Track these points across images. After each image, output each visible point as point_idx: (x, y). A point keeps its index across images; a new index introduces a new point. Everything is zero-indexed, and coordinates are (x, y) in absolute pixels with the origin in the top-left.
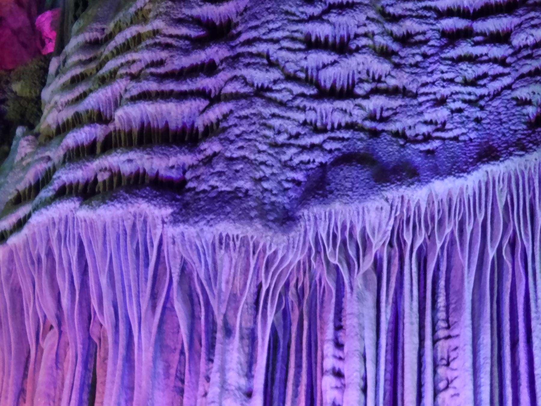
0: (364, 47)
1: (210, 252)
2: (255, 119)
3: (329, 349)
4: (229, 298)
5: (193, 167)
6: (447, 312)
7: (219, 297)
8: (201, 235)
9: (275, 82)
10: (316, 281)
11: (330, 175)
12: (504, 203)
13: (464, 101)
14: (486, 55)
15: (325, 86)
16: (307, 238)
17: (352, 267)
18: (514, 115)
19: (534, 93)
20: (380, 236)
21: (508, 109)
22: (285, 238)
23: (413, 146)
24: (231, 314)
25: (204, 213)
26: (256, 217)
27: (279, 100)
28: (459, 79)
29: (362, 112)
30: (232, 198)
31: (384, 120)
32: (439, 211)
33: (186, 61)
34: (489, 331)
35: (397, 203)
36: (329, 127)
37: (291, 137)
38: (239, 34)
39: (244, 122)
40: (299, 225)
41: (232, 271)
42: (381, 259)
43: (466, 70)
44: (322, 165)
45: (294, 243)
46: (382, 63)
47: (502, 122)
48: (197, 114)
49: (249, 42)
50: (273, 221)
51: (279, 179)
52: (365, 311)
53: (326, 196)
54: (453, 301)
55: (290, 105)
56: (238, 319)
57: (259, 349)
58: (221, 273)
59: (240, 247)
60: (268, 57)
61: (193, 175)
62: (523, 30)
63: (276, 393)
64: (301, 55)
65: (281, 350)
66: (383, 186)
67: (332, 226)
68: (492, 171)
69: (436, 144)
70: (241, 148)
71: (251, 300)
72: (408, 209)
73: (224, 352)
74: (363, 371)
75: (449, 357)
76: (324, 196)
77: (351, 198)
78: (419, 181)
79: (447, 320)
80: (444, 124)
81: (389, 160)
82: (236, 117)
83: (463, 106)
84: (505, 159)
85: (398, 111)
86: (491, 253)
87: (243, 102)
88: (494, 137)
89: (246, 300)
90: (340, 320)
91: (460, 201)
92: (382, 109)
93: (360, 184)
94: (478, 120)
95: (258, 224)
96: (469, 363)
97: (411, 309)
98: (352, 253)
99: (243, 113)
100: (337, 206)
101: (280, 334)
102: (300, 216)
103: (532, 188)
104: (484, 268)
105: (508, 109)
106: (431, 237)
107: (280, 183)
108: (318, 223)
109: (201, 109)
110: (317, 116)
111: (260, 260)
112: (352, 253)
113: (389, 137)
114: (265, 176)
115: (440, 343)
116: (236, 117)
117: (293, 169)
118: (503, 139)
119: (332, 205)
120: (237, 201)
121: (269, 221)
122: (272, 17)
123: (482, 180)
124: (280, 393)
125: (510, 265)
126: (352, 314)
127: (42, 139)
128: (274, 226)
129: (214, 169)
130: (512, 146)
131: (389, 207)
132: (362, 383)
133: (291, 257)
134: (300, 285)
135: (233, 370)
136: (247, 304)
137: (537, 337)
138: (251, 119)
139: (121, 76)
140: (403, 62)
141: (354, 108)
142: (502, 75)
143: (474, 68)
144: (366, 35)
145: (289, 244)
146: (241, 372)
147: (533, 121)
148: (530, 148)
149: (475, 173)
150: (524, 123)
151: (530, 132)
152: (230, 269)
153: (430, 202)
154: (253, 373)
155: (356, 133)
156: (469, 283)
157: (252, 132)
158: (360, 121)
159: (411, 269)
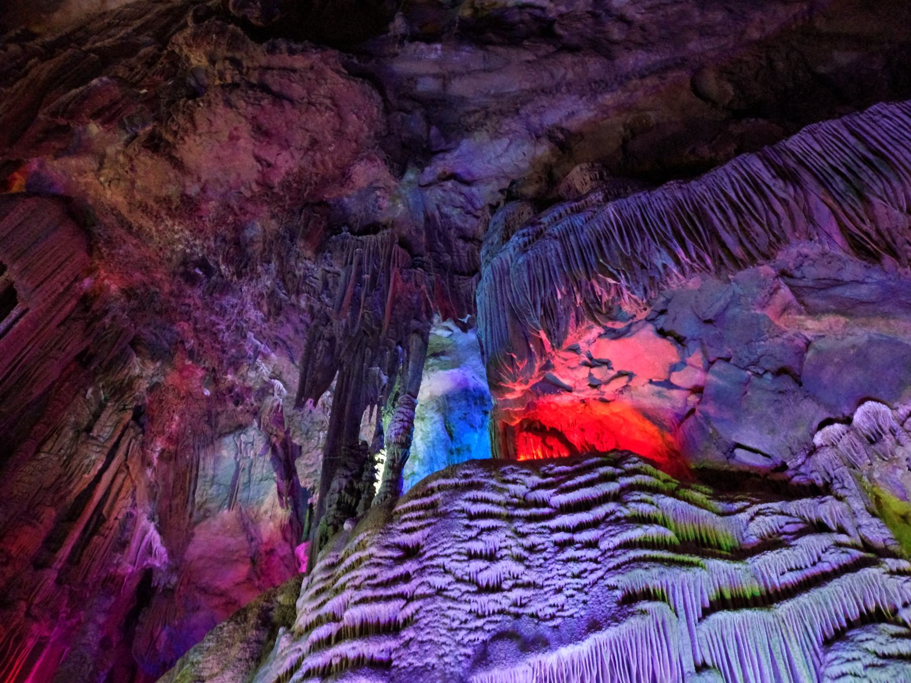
0: (506, 555)
2: (437, 611)
5: (396, 650)
9: (449, 584)
11: (489, 649)
13: (574, 589)
28: (569, 574)
31: (523, 606)
33: (390, 574)
35: (537, 666)
36: (487, 613)
37: (461, 623)
38: (425, 552)
39: (429, 614)
44: (484, 642)
49: (431, 558)
60: (444, 567)
62: (606, 539)
64: (465, 564)
69: (558, 621)
72: (545, 671)
76: (487, 665)
87: (429, 600)
94: (585, 602)
99: (429, 608)
113: (527, 618)
117: (464, 646)
122: (445, 540)
127: (295, 635)
139: (349, 588)
142: (596, 569)
144: (506, 547)
149: (587, 641)
153: (559, 664)
158: (507, 608)
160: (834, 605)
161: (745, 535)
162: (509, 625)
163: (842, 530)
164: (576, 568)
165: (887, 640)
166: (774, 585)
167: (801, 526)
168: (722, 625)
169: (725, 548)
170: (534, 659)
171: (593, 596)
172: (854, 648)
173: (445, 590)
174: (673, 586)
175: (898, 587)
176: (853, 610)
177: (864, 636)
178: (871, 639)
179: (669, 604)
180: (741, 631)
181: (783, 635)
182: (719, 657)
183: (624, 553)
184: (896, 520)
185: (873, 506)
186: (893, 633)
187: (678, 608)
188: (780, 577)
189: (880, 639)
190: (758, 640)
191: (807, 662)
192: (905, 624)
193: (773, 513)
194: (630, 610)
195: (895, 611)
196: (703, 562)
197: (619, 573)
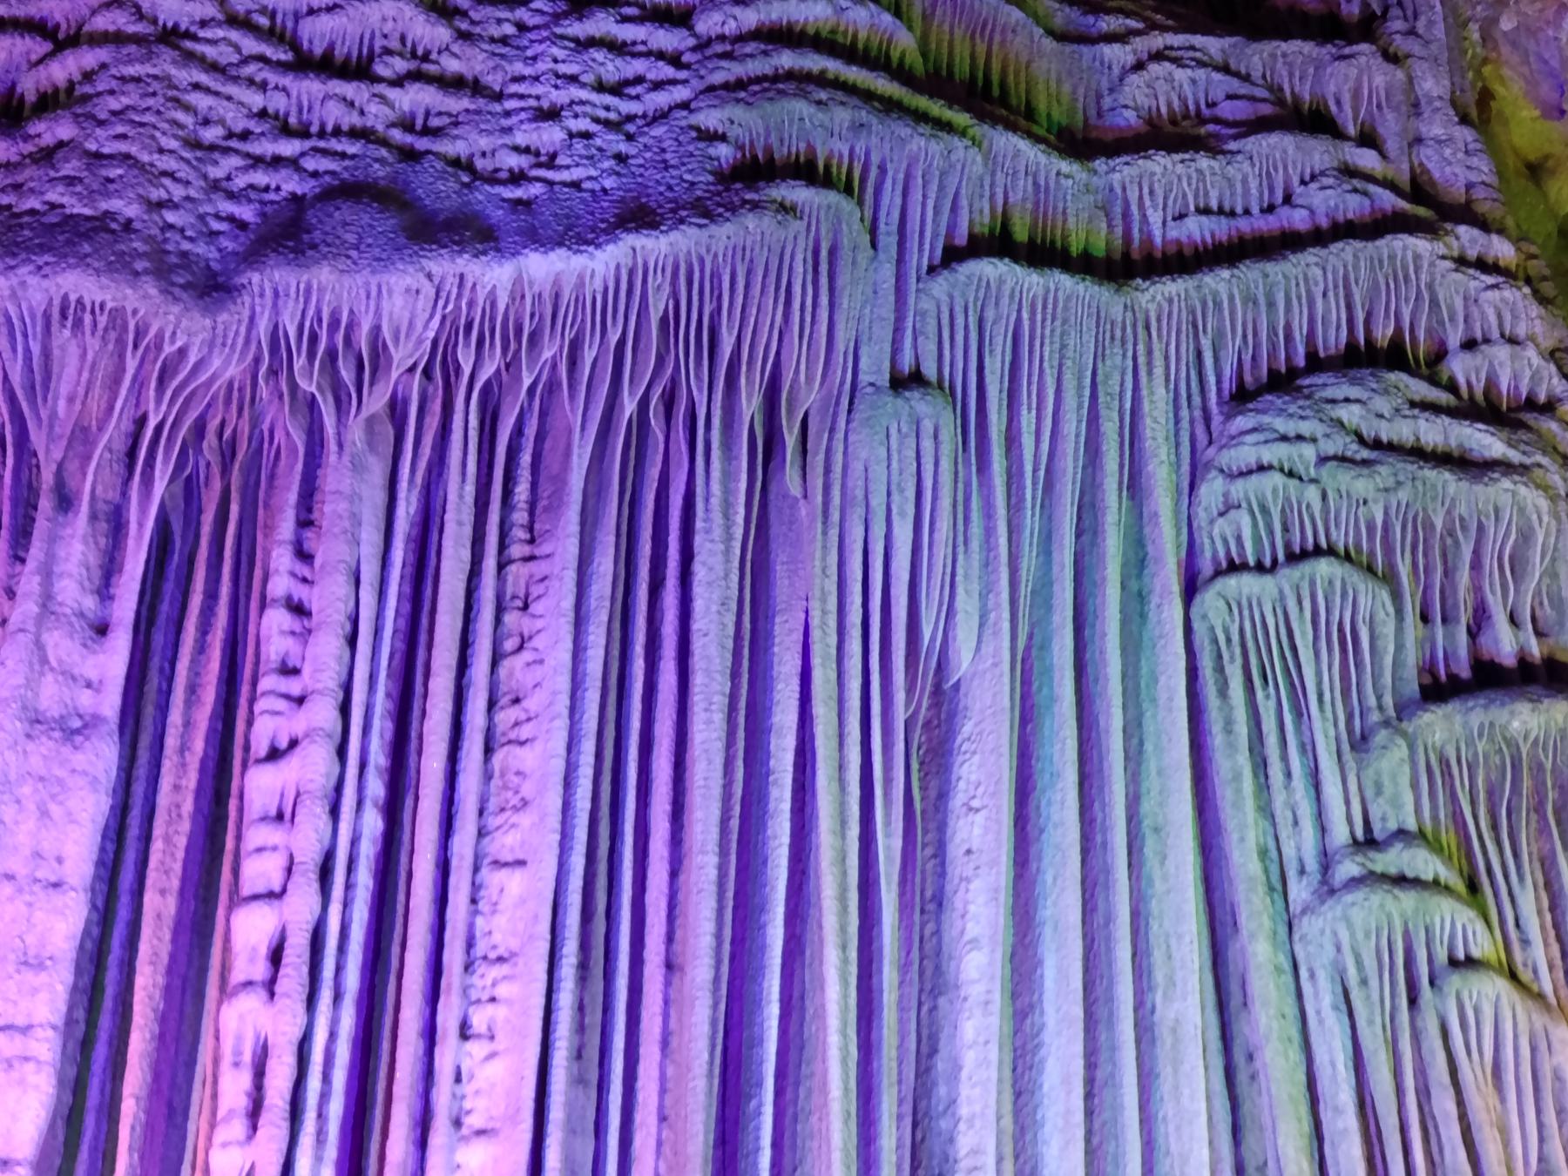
2: (156, 86)
3: (282, 559)
4: (73, 432)
6: (532, 513)
7: (51, 427)
8: (20, 293)
9: (203, 24)
11: (311, 217)
12: (661, 313)
13: (597, 120)
14: (644, 43)
15: (311, 51)
17: (344, 405)
18: (691, 155)
19: (732, 122)
20: (411, 345)
21: (680, 144)
22: (208, 322)
23: (487, 187)
24: (72, 466)
25: (28, 250)
26: (146, 272)
27: (209, 60)
28: (588, 78)
29: (387, 110)
30: (95, 230)
31: (436, 133)
32: (532, 315)
34: (612, 551)
35: (451, 285)
36: (314, 129)
37: (230, 135)
39: (131, 87)
41: (86, 375)
42: (406, 402)
43: (602, 64)
44: (295, 198)
45: (225, 336)
47: (667, 166)
48: (25, 67)
50: (184, 287)
51: (201, 210)
52: (366, 492)
53: (303, 253)
54: (545, 494)
56: (90, 478)
57: (131, 542)
58: (59, 378)
59: (106, 330)
63: (159, 639)
66: (423, 249)
67: (311, 312)
68: (643, 247)
69: (536, 189)
70: (123, 137)
71: (120, 446)
72: (471, 304)
73: (52, 539)
74: (352, 603)
76: (299, 251)
77: (355, 263)
78: (498, 250)
79: (530, 528)
80: (553, 156)
83: (594, 128)
84: (671, 229)
85: (460, 119)
86: (629, 407)
88: (650, 191)
89: (109, 441)
90: (310, 510)
92: (427, 114)
93: (376, 238)
94: (621, 158)
96: (568, 603)
97: (461, 497)
98: (347, 374)
99: (131, 70)
100: (323, 274)
101: (177, 526)
102: (243, 286)
104: (612, 433)
105: (680, 144)
106: (512, 366)
107: (202, 218)
109: (34, 57)
111: (147, 366)
112: (347, 374)
113: (439, 165)
115: (513, 568)
117: (231, 196)
118: (669, 194)
119: (315, 270)
120: (107, 236)
121: (173, 284)
123: (623, 263)
125: (661, 438)
126: (337, 492)
128: (185, 296)
129: (57, 171)
130: (684, 209)
131: (434, 291)
132: (348, 627)
133: (216, 363)
135: (70, 576)
136: (110, 451)
137: (704, 564)
138: (148, 84)
140: (477, 30)
141: (369, 101)
142: (673, 82)
143: (619, 62)
145: (214, 336)
146: (87, 583)
148: (720, 215)
149: (610, 248)
150: (710, 172)
151: (720, 188)
152: (80, 374)
153: (517, 295)
154: (112, 591)
156: (580, 456)
157: (148, 109)
158: (380, 128)
161: (1107, 102)
162: (379, 171)
163: (1368, 139)
164: (612, 68)
165: (1397, 410)
166: (1148, 238)
167: (1266, 109)
170: (446, 266)
172: (1308, 412)
173: (194, 38)
174: (882, 169)
175: (1465, 299)
178: (1358, 401)
179: (861, 203)
181: (1135, 359)
182: (959, 367)
183: (765, 53)
185: (1470, 98)
186: (1417, 398)
187: (882, 227)
188: (1170, 223)
189: (1382, 404)
190: (1070, 354)
191: (1177, 434)
192: (1452, 387)
193: (1201, 64)
194: (748, 197)
195: (1440, 354)
196: (981, 130)
197: (738, 101)
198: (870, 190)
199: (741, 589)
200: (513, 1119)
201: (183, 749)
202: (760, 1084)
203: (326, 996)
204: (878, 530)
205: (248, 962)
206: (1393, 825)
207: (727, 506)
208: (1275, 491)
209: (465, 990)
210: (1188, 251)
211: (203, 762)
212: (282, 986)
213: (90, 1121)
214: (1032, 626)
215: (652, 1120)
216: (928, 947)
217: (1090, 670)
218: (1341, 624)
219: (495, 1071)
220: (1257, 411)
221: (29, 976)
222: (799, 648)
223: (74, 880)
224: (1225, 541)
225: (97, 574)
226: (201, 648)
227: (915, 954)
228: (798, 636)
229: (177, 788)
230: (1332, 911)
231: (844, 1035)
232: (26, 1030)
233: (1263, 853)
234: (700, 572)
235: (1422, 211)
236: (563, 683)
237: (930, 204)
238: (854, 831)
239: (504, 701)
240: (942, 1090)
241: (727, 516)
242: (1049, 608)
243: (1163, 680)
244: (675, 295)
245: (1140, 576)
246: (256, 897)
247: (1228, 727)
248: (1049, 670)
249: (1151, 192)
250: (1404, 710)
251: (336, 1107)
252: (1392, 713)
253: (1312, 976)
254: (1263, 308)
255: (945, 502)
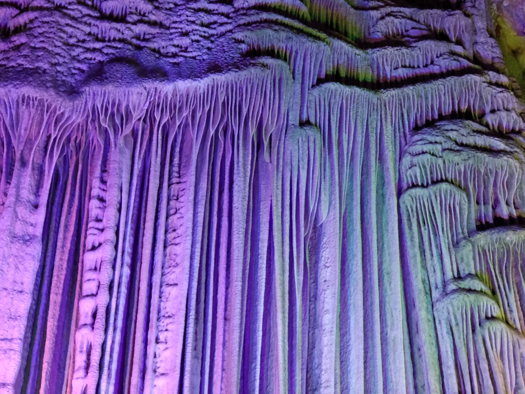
1: (15, 106)
2: (54, 25)
3: (96, 183)
4: (26, 140)
7: (19, 139)
8: (9, 94)
10: (89, 141)
11: (106, 68)
13: (201, 36)
14: (217, 10)
15: (106, 13)
16: (87, 107)
17: (117, 131)
18: (233, 48)
20: (139, 111)
21: (229, 44)
22: (71, 104)
23: (165, 59)
24: (26, 152)
26: (51, 87)
28: (198, 22)
29: (130, 33)
30: (34, 73)
31: (148, 40)
32: (180, 101)
34: (206, 180)
35: (152, 91)
36: (107, 39)
37: (79, 41)
39: (45, 25)
40: (82, 97)
41: (30, 121)
42: (138, 130)
43: (203, 17)
44: (100, 62)
45: (77, 108)
46: (146, 4)
48: (10, 18)
50: (63, 92)
51: (69, 66)
52: (124, 161)
53: (103, 81)
54: (184, 161)
55: (80, 20)
57: (46, 177)
59: (37, 106)
61: (5, 56)
63: (55, 210)
65: (61, 182)
66: (143, 79)
67: (106, 100)
68: (217, 79)
69: (181, 59)
70: (43, 42)
71: (42, 145)
72: (159, 98)
73: (19, 177)
74: (119, 198)
75: (178, 195)
76: (102, 80)
77: (120, 84)
78: (168, 80)
80: (187, 48)
81: (148, 65)
82: (40, 22)
83: (200, 39)
84: (226, 73)
85: (156, 36)
86: (212, 132)
87: (46, 12)
89: (38, 143)
90: (105, 167)
91: (194, 96)
92: (145, 34)
94: (209, 49)
95: (52, 92)
96: (192, 198)
97: (156, 162)
98: (118, 121)
99: (45, 19)
100: (110, 88)
101: (61, 172)
102: (83, 92)
103: (241, 94)
105: (229, 44)
106: (173, 118)
107: (69, 69)
108: (96, 97)
109: (13, 15)
110: (99, 31)
111: (51, 119)
112: (118, 121)
113: (148, 51)
114: (59, 63)
116: (40, 22)
117: (79, 61)
119: (107, 86)
120: (37, 75)
121: (60, 91)
123: (210, 84)
124: (57, 211)
125: (223, 142)
128: (64, 95)
129: (21, 53)
131: (147, 93)
133: (74, 117)
134: (78, 141)
135: (26, 188)
136: (39, 147)
140: (161, 6)
141: (125, 30)
142: (227, 23)
143: (208, 16)
145: (73, 108)
147: (245, 53)
148: (242, 68)
149: (206, 79)
150: (239, 54)
152: (29, 121)
153: (174, 95)
155: (126, 45)
156: (196, 149)
157: (51, 32)
158: (129, 39)
159: (158, 137)
160: (432, 100)
161: (372, 30)
163: (459, 42)
164: (206, 19)
166: (385, 76)
167: (425, 32)
168: (332, 94)
169: (350, 36)
170: (151, 85)
171: (218, 45)
172: (439, 134)
173: (67, 8)
174: (297, 52)
175: (492, 96)
176: (447, 107)
177: (451, 126)
178: (455, 130)
179: (289, 64)
180: (347, 103)
182: (322, 118)
183: (258, 14)
184: (507, 50)
185: (493, 29)
186: (475, 129)
187: (297, 72)
188: (393, 71)
189: (464, 131)
191: (395, 142)
192: (487, 126)
193: (403, 17)
196: (329, 39)
197: (248, 30)
198: (292, 60)
199: (249, 193)
200: (173, 370)
201: (63, 246)
202: (256, 358)
203: (111, 328)
204: (295, 174)
205: (85, 317)
206: (467, 272)
207: (245, 165)
208: (428, 160)
209: (157, 327)
210: (399, 80)
211: (70, 251)
212: (96, 325)
213: (32, 370)
214: (347, 205)
215: (220, 370)
216: (311, 313)
217: (366, 220)
218: (450, 207)
219: (167, 353)
220: (422, 134)
221: (12, 322)
222: (268, 213)
223: (27, 290)
224: (411, 177)
225: (34, 188)
226: (69, 213)
227: (307, 315)
228: (269, 209)
229: (61, 259)
230: (447, 301)
231: (284, 342)
232: (11, 340)
233: (424, 282)
234: (236, 188)
235: (477, 67)
236: (190, 224)
237: (313, 64)
238: (287, 274)
239: (170, 230)
240: (316, 360)
241: (244, 169)
242: (352, 200)
243: (390, 224)
244: (227, 95)
245: (382, 189)
246: (87, 296)
247: (412, 240)
248: (352, 220)
249: (387, 60)
250: (471, 233)
251: (114, 366)
252: (467, 234)
253: (440, 322)
254: (424, 99)
255: (318, 164)
